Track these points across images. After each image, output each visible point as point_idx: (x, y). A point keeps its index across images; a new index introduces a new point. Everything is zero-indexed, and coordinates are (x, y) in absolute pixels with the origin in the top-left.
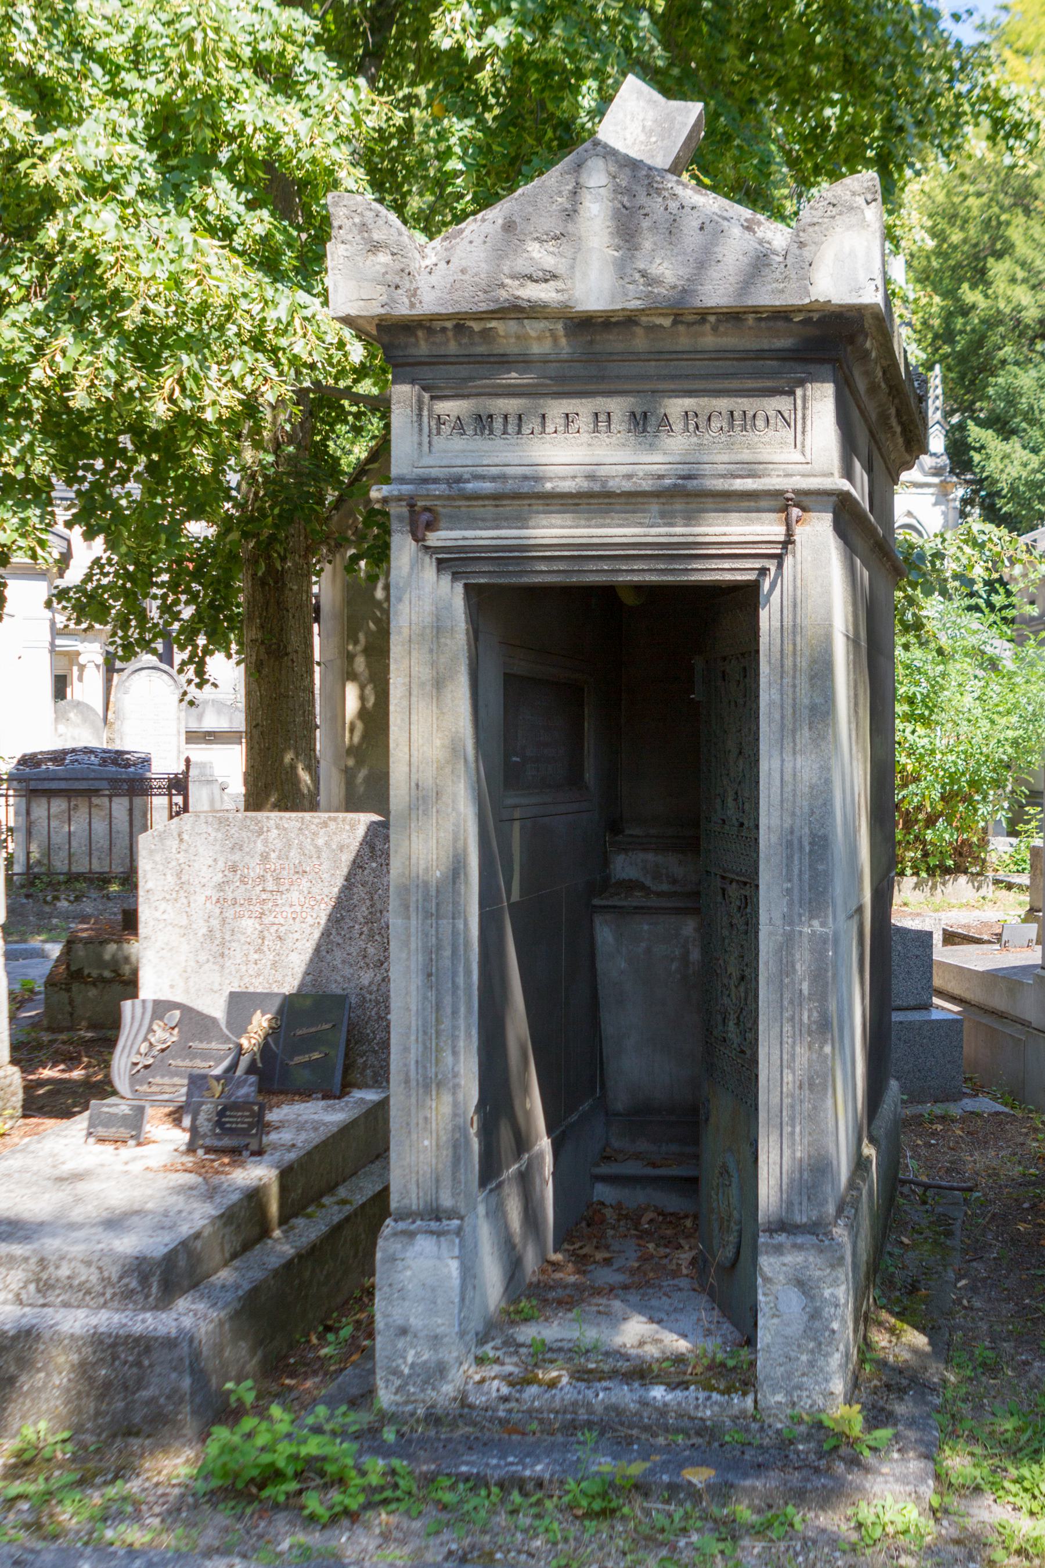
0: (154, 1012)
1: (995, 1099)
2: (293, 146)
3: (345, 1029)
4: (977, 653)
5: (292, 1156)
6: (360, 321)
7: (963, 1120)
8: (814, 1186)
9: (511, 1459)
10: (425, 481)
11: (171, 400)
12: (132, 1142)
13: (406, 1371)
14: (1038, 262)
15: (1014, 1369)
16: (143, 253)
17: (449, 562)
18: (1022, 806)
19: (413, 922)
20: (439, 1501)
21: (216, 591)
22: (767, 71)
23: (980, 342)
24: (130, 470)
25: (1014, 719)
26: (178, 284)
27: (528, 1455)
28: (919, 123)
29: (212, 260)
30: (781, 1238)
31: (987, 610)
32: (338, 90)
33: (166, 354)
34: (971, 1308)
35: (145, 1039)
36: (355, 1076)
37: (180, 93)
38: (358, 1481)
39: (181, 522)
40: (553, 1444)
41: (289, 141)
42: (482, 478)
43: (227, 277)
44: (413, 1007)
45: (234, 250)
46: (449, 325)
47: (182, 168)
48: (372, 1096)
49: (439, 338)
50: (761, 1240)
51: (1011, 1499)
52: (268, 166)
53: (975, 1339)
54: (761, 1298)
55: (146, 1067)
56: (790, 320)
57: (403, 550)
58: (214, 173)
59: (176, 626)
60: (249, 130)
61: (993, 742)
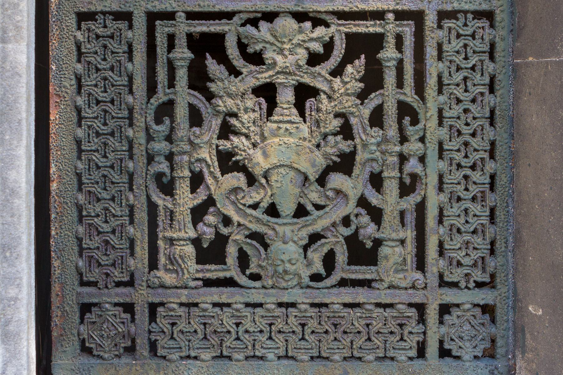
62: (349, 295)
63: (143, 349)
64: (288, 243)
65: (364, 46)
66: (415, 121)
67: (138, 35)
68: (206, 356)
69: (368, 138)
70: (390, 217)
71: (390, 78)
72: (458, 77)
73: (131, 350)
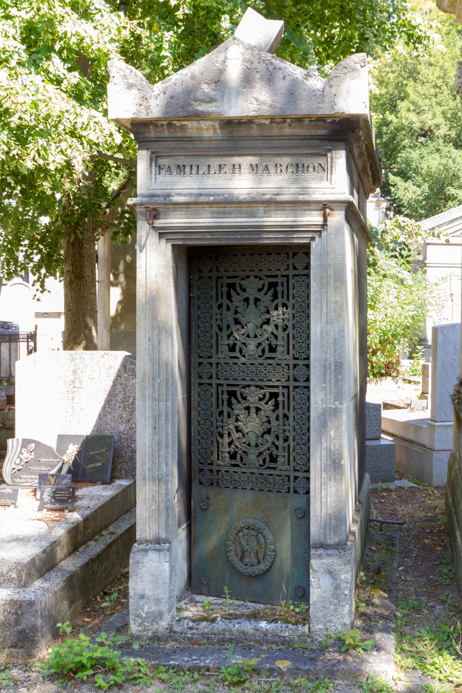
0: (23, 444)
1: (409, 480)
2: (90, 43)
3: (112, 452)
4: (395, 277)
5: (88, 512)
6: (123, 121)
7: (396, 490)
8: (336, 527)
9: (194, 657)
10: (153, 196)
11: (34, 160)
12: (12, 506)
13: (144, 616)
14: (420, 102)
15: (428, 610)
16: (20, 91)
17: (163, 234)
18: (415, 346)
19: (147, 403)
20: (160, 679)
21: (50, 248)
22: (306, 13)
23: (394, 138)
24: (12, 192)
25: (412, 307)
26: (36, 106)
27: (202, 656)
28: (375, 36)
29: (52, 96)
30: (321, 551)
31: (400, 258)
32: (110, 17)
33: (30, 138)
34: (406, 581)
35: (19, 457)
36: (117, 474)
37: (37, 18)
38: (121, 670)
39: (37, 217)
40: (214, 649)
41: (87, 40)
42: (180, 195)
43: (58, 103)
44: (147, 444)
45: (62, 90)
46: (165, 123)
47: (37, 52)
48: (125, 483)
49: (160, 129)
50: (312, 552)
51: (430, 673)
52: (78, 53)
53: (408, 595)
54: (311, 579)
55: (19, 470)
56: (325, 121)
57: (143, 228)
58: (53, 55)
59: (32, 264)
60: (69, 35)
61: (403, 317)
62: (269, 471)
63: (215, 484)
64: (252, 345)
65: (274, 396)
66: (288, 420)
67: (214, 390)
68: (231, 487)
69: (274, 423)
70: (280, 337)
71: (280, 295)
72: (299, 407)
73: (212, 484)
